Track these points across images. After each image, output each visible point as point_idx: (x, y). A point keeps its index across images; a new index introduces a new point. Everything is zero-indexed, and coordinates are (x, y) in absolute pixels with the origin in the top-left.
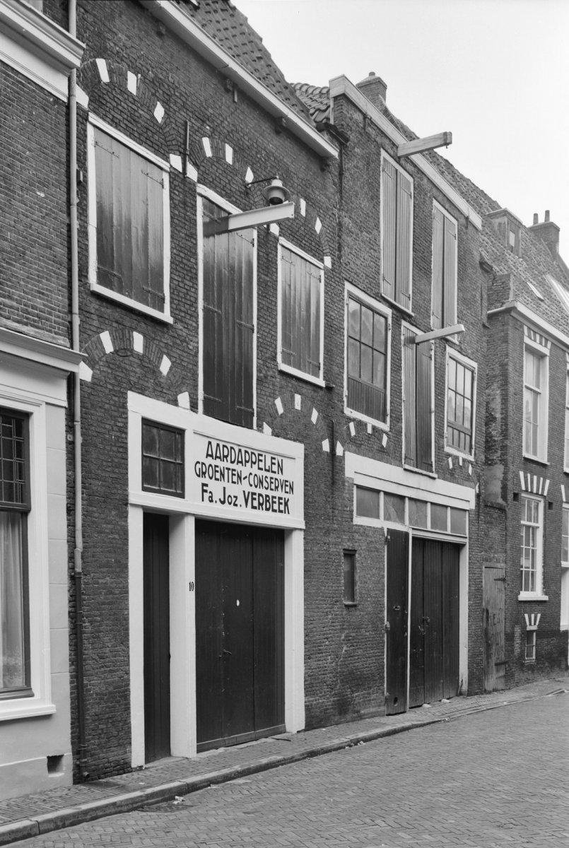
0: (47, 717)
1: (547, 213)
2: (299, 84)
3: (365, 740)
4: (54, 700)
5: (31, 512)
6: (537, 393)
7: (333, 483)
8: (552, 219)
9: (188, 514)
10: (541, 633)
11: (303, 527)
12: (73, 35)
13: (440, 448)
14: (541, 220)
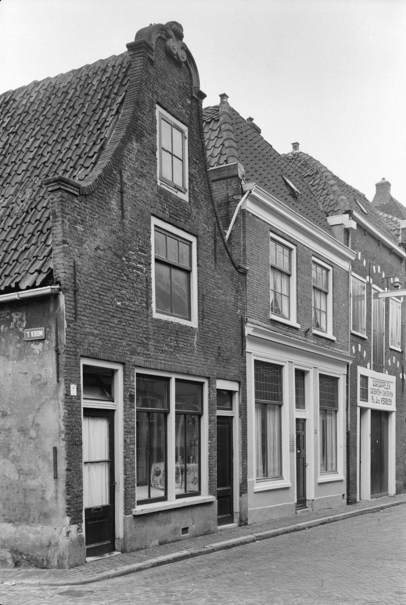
0: (287, 488)
2: (326, 168)
4: (291, 481)
5: (170, 413)
9: (369, 408)
11: (396, 410)
12: (350, 248)
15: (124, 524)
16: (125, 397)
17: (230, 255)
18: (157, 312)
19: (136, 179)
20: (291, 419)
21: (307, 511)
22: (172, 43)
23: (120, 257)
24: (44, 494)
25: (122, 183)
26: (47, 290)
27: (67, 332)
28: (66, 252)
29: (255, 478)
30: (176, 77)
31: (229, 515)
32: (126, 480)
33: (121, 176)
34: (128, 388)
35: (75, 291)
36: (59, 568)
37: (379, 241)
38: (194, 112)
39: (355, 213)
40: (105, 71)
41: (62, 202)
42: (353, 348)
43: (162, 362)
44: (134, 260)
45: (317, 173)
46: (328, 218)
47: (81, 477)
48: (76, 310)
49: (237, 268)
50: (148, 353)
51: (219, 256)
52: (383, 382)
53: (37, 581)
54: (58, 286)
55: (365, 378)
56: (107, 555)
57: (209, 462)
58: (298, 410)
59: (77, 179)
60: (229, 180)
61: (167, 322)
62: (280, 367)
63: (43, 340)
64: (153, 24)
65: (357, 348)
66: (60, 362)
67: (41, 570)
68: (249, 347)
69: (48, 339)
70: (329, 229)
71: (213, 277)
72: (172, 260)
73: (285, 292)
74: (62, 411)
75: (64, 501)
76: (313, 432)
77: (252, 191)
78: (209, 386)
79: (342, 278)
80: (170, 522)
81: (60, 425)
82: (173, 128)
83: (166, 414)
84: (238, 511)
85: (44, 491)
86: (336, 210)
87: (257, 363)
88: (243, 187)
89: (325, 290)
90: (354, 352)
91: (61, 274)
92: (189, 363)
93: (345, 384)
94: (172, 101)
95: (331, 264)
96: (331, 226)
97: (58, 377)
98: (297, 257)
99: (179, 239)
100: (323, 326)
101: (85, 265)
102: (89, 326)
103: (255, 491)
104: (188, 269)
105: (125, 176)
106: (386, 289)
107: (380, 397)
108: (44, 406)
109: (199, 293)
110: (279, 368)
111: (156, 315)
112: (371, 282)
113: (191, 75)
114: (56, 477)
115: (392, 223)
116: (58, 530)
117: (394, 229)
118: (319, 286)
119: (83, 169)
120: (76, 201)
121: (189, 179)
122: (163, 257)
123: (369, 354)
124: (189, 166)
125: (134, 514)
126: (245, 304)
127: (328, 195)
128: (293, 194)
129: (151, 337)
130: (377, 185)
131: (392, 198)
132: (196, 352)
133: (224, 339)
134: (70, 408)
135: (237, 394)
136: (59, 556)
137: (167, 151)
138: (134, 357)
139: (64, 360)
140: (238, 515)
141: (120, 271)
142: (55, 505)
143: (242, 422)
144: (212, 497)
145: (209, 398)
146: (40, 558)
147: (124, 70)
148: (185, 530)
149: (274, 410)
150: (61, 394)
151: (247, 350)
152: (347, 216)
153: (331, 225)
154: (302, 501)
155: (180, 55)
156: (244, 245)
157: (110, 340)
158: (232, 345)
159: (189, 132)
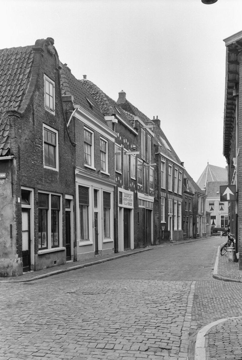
0: (91, 245)
1: (157, 116)
2: (102, 91)
3: (146, 251)
4: (93, 242)
6: (163, 172)
7: (136, 199)
8: (159, 118)
10: (164, 231)
11: (133, 208)
12: (115, 132)
13: (149, 189)
14: (156, 118)
15: (35, 258)
16: (35, 202)
17: (69, 137)
18: (45, 165)
19: (38, 107)
20: (92, 212)
21: (99, 256)
22: (50, 47)
23: (33, 142)
24: (5, 245)
25: (33, 110)
26: (9, 157)
27: (17, 175)
28: (16, 141)
29: (79, 240)
30: (51, 61)
31: (69, 256)
32: (35, 239)
33: (33, 107)
34: (36, 199)
35: (19, 158)
36: (13, 276)
37: (126, 127)
38: (57, 75)
39: (117, 115)
40: (17, 54)
41: (14, 121)
42: (116, 178)
43: (47, 187)
44: (38, 143)
45: (97, 93)
46: (105, 117)
47: (21, 237)
48: (19, 166)
49: (72, 144)
50: (42, 183)
51: (66, 139)
52: (129, 195)
53: (8, 281)
54: (13, 156)
55: (121, 193)
56: (29, 272)
57: (63, 232)
58: (95, 208)
59: (13, 106)
60: (67, 103)
61: (48, 170)
62: (88, 188)
63: (5, 178)
64: (67, 66)
65: (118, 178)
66: (14, 188)
67: (4, 278)
68: (77, 179)
69: (7, 178)
70: (105, 122)
71: (64, 149)
72: (49, 142)
73: (89, 153)
74: (15, 209)
75: (16, 247)
76: (101, 218)
77: (78, 109)
78: (63, 198)
79: (111, 145)
80: (50, 258)
81: (13, 215)
82: (50, 84)
83: (47, 210)
84: (73, 254)
85: (5, 244)
86: (108, 113)
87: (79, 186)
88: (74, 106)
89: (90, 144)
90: (117, 180)
91: (14, 151)
92: (56, 188)
93: (113, 196)
94: (49, 72)
95: (107, 139)
96: (106, 121)
97: (13, 194)
98: (94, 137)
99: (52, 132)
100: (104, 168)
101: (22, 147)
102: (23, 173)
103: (80, 245)
104: (55, 145)
105: (34, 107)
106: (129, 150)
107: (127, 202)
108: (5, 207)
109: (59, 156)
110: (87, 189)
111: (45, 167)
112: (123, 147)
113: (56, 59)
114: (11, 237)
115: (130, 117)
116: (13, 260)
117: (131, 120)
118: (88, 142)
119: (15, 102)
120: (19, 120)
121: (55, 105)
122: (46, 141)
123: (122, 181)
124: (55, 99)
125: (38, 254)
126: (75, 160)
127: (103, 105)
128: (91, 107)
129: (43, 176)
130: (120, 94)
131: (127, 101)
132: (58, 182)
133: (67, 177)
134: (18, 208)
135: (72, 201)
136: (13, 271)
137: (48, 94)
138: (38, 185)
139: (15, 187)
140: (33, 267)
141: (33, 148)
142: (11, 249)
143: (75, 214)
144: (64, 248)
145: (63, 203)
146: (3, 273)
147: (28, 56)
148: (55, 262)
149: (85, 208)
150: (14, 202)
151: (76, 181)
152: (113, 117)
153: (106, 120)
154: (97, 252)
155: (53, 52)
156: (74, 133)
157: (30, 179)
158: (70, 179)
159: (55, 84)
